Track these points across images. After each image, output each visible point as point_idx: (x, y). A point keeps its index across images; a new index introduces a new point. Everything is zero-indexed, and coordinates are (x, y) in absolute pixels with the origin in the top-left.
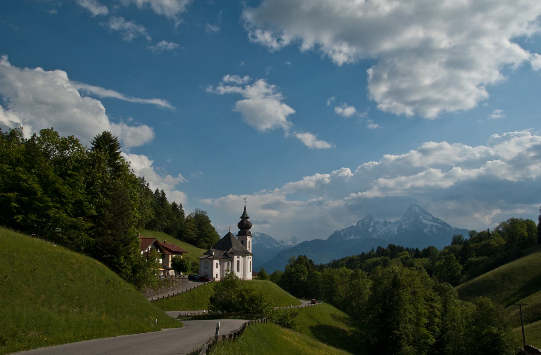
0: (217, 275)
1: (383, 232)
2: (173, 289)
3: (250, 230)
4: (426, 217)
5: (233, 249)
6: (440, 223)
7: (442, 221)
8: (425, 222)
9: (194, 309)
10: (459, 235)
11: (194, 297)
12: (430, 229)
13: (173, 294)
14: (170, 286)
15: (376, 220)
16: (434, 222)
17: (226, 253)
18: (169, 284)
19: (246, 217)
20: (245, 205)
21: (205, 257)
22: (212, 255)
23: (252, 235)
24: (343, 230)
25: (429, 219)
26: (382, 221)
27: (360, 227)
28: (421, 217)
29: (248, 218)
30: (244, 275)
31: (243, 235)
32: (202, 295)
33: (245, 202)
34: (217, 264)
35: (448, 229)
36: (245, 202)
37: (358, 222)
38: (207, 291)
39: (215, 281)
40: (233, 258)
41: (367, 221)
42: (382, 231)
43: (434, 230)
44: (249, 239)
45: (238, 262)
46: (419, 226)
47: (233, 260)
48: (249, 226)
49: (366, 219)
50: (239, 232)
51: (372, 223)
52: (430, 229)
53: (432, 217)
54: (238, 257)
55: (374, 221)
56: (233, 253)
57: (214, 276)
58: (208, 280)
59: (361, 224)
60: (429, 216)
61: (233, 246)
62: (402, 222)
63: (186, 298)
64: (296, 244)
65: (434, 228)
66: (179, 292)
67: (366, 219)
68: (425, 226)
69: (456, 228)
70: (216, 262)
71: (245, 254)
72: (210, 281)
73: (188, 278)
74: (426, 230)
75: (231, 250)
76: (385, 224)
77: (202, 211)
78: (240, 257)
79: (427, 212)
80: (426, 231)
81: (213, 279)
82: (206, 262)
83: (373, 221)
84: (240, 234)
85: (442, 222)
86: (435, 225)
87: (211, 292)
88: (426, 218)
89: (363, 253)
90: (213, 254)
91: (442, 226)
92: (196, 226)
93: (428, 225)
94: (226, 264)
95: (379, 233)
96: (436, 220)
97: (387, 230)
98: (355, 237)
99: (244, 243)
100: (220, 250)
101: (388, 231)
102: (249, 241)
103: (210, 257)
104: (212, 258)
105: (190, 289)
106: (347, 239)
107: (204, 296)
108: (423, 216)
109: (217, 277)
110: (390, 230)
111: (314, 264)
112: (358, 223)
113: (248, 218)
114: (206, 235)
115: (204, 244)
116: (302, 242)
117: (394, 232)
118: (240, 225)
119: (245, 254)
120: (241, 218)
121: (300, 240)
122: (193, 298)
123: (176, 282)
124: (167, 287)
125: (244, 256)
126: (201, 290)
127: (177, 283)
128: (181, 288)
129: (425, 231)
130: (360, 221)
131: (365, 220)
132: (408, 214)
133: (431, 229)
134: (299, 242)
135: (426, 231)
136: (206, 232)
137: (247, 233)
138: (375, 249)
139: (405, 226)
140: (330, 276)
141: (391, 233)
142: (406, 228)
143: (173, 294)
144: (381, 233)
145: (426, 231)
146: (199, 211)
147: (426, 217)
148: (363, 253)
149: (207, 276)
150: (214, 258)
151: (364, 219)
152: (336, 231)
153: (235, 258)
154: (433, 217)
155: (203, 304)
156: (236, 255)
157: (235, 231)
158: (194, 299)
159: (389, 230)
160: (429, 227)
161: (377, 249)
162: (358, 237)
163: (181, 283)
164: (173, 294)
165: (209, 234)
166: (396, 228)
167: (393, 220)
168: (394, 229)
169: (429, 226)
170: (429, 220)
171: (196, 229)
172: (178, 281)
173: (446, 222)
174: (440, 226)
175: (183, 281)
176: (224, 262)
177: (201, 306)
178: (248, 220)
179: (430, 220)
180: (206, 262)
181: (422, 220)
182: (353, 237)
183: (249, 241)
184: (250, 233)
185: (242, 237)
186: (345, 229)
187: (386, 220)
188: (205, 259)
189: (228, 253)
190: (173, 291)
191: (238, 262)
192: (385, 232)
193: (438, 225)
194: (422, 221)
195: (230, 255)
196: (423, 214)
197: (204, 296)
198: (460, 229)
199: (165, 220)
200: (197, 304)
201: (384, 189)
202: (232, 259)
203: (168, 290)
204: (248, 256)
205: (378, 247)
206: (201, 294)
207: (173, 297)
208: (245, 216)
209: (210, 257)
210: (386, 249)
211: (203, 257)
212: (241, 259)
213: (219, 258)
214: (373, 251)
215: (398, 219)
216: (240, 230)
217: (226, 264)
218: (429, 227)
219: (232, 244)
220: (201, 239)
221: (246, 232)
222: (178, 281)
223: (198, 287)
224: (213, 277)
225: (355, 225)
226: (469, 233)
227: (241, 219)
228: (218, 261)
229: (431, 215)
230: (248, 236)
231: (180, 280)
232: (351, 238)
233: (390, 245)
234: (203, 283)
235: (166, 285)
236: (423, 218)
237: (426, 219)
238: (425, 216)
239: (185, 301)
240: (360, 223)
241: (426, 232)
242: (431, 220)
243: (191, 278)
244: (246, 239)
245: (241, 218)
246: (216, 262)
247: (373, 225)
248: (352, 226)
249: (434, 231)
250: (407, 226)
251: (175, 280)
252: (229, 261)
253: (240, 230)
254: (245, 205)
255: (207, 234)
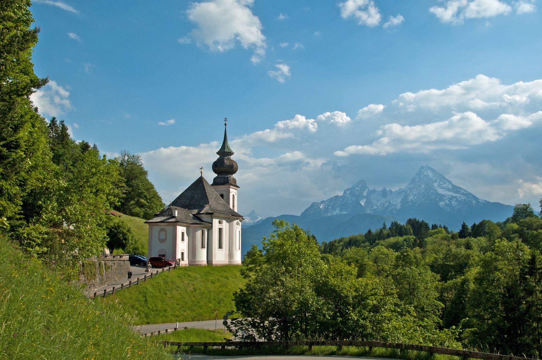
0: (182, 254)
1: (381, 205)
2: (102, 282)
3: (234, 176)
4: (442, 184)
5: (210, 206)
6: (463, 194)
7: (465, 191)
8: (441, 191)
9: (149, 321)
10: (524, 205)
11: (145, 297)
12: (448, 202)
13: (105, 291)
14: (95, 275)
15: (371, 188)
16: (454, 193)
17: (199, 213)
18: (93, 272)
19: (228, 152)
20: (225, 131)
21: (160, 220)
22: (175, 217)
23: (238, 184)
24: (323, 202)
25: (446, 187)
26: (379, 189)
27: (348, 197)
28: (436, 185)
29: (231, 153)
30: (231, 255)
31: (223, 184)
32: (161, 292)
33: (225, 125)
34: (183, 233)
35: (474, 202)
36: (225, 125)
37: (345, 191)
38: (170, 284)
39: (180, 266)
40: (212, 223)
41: (358, 189)
42: (379, 204)
43: (454, 203)
44: (233, 191)
45: (220, 230)
46: (432, 198)
47: (212, 227)
48: (232, 169)
49: (357, 186)
50: (215, 179)
51: (365, 192)
52: (448, 202)
53: (451, 185)
54: (220, 222)
55: (369, 190)
56: (211, 214)
57: (179, 256)
58: (168, 264)
59: (350, 194)
60: (448, 183)
61: (209, 200)
62: (409, 192)
63: (130, 299)
64: (256, 221)
65: (454, 200)
66: (116, 288)
67: (357, 186)
68: (442, 197)
69: (485, 201)
70: (181, 229)
71: (232, 215)
72: (171, 265)
73: (129, 260)
74: (442, 204)
75: (206, 209)
76: (384, 193)
77: (133, 156)
78: (224, 221)
79: (444, 178)
80: (442, 205)
81: (176, 261)
82: (162, 230)
83: (367, 190)
84: (216, 183)
85: (465, 192)
86: (455, 197)
87: (178, 287)
88: (443, 186)
89: (369, 232)
90: (176, 215)
91: (465, 198)
92: (123, 178)
93: (446, 197)
94: (199, 233)
95: (375, 207)
96: (456, 189)
97: (386, 203)
98: (341, 212)
99: (224, 196)
100: (186, 208)
101: (387, 204)
102: (233, 195)
103: (170, 221)
104: (174, 222)
105: (136, 280)
106: (329, 214)
107: (166, 294)
108: (439, 183)
109: (183, 259)
110: (390, 203)
111: (184, 266)
112: (345, 193)
113: (231, 153)
114: (140, 195)
115: (137, 209)
116: (264, 218)
117: (396, 206)
118: (217, 166)
119: (231, 216)
120: (218, 153)
121: (260, 216)
122: (144, 299)
123: (107, 268)
124: (89, 278)
125: (229, 220)
126: (158, 283)
127: (109, 270)
128: (117, 279)
129: (440, 204)
130: (347, 190)
131: (355, 188)
132: (417, 180)
133: (450, 201)
134: (260, 218)
135: (443, 204)
136: (141, 190)
137: (230, 180)
138: (388, 226)
139: (412, 197)
140: (358, 260)
141: (392, 207)
142: (414, 200)
143: (103, 292)
144: (378, 206)
145: (443, 204)
146: (128, 156)
147: (442, 184)
148: (369, 232)
149: (164, 256)
150: (178, 222)
151: (353, 186)
152: (313, 203)
153: (216, 222)
154: (453, 185)
155: (165, 311)
156: (217, 217)
157: (210, 176)
158: (146, 300)
159: (389, 202)
160: (446, 199)
161: (391, 226)
162: (345, 213)
163: (116, 269)
164: (105, 291)
165: (146, 194)
166: (399, 200)
167: (394, 189)
168: (396, 201)
169: (447, 198)
170: (446, 189)
171: (124, 185)
172: (111, 266)
173: (471, 193)
174: (463, 198)
175: (120, 265)
176: (195, 231)
177: (161, 314)
178: (232, 157)
179: (449, 190)
180: (162, 230)
181: (436, 189)
182: (337, 212)
183: (233, 195)
184: (235, 181)
185: (222, 188)
186: (326, 201)
187: (385, 189)
188: (160, 224)
189: (202, 214)
190: (102, 284)
191: (220, 230)
192: (384, 206)
193: (460, 197)
194: (437, 190)
195: (205, 218)
196: (438, 180)
197: (166, 294)
198: (491, 203)
199: (69, 168)
200: (153, 311)
201: (398, 140)
202: (211, 225)
203: (91, 283)
204: (237, 221)
205: (392, 223)
206: (160, 291)
207: (104, 296)
208: (227, 150)
209: (170, 221)
210: (405, 225)
211: (157, 221)
212: (225, 225)
213: (187, 223)
214: (384, 228)
215: (403, 186)
216: (216, 175)
217: (199, 233)
218: (446, 199)
219: (208, 197)
220: (132, 202)
221: (228, 178)
222: (111, 266)
223: (151, 276)
224: (177, 258)
225: (341, 194)
226: (540, 202)
227: (218, 156)
228: (185, 228)
229: (450, 182)
230: (231, 187)
231: (114, 264)
232: (335, 213)
233: (410, 220)
234: (160, 270)
235: (88, 273)
236: (438, 186)
237: (443, 188)
238: (442, 183)
239: (128, 305)
240: (348, 192)
241: (442, 207)
242: (451, 188)
243: (134, 261)
244: (228, 192)
245: (218, 153)
246: (181, 229)
247: (367, 195)
248: (337, 197)
249: (454, 205)
250: (415, 198)
251: (105, 264)
252: (205, 227)
253: (216, 175)
254: (225, 131)
255: (142, 193)
